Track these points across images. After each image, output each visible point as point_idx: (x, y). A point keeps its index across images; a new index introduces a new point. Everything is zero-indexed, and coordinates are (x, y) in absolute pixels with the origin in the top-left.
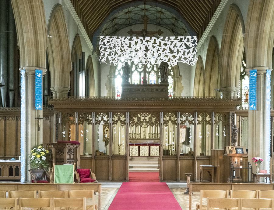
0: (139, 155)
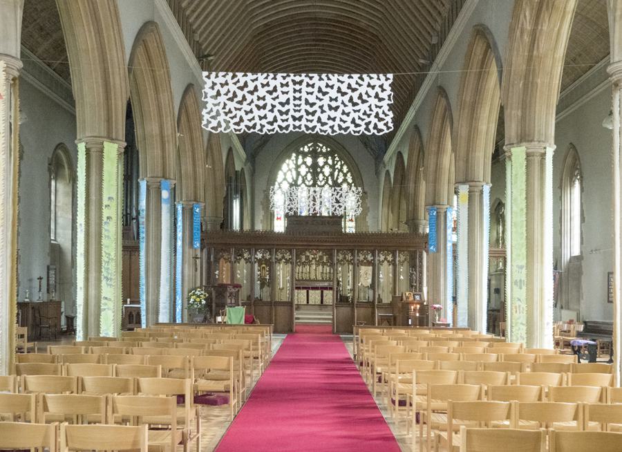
0: (308, 302)
